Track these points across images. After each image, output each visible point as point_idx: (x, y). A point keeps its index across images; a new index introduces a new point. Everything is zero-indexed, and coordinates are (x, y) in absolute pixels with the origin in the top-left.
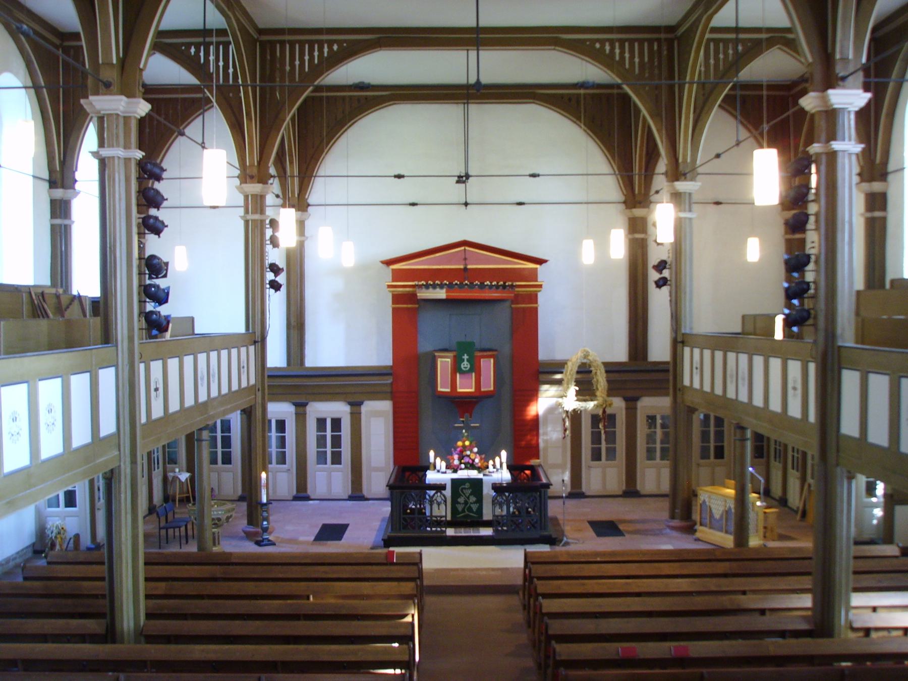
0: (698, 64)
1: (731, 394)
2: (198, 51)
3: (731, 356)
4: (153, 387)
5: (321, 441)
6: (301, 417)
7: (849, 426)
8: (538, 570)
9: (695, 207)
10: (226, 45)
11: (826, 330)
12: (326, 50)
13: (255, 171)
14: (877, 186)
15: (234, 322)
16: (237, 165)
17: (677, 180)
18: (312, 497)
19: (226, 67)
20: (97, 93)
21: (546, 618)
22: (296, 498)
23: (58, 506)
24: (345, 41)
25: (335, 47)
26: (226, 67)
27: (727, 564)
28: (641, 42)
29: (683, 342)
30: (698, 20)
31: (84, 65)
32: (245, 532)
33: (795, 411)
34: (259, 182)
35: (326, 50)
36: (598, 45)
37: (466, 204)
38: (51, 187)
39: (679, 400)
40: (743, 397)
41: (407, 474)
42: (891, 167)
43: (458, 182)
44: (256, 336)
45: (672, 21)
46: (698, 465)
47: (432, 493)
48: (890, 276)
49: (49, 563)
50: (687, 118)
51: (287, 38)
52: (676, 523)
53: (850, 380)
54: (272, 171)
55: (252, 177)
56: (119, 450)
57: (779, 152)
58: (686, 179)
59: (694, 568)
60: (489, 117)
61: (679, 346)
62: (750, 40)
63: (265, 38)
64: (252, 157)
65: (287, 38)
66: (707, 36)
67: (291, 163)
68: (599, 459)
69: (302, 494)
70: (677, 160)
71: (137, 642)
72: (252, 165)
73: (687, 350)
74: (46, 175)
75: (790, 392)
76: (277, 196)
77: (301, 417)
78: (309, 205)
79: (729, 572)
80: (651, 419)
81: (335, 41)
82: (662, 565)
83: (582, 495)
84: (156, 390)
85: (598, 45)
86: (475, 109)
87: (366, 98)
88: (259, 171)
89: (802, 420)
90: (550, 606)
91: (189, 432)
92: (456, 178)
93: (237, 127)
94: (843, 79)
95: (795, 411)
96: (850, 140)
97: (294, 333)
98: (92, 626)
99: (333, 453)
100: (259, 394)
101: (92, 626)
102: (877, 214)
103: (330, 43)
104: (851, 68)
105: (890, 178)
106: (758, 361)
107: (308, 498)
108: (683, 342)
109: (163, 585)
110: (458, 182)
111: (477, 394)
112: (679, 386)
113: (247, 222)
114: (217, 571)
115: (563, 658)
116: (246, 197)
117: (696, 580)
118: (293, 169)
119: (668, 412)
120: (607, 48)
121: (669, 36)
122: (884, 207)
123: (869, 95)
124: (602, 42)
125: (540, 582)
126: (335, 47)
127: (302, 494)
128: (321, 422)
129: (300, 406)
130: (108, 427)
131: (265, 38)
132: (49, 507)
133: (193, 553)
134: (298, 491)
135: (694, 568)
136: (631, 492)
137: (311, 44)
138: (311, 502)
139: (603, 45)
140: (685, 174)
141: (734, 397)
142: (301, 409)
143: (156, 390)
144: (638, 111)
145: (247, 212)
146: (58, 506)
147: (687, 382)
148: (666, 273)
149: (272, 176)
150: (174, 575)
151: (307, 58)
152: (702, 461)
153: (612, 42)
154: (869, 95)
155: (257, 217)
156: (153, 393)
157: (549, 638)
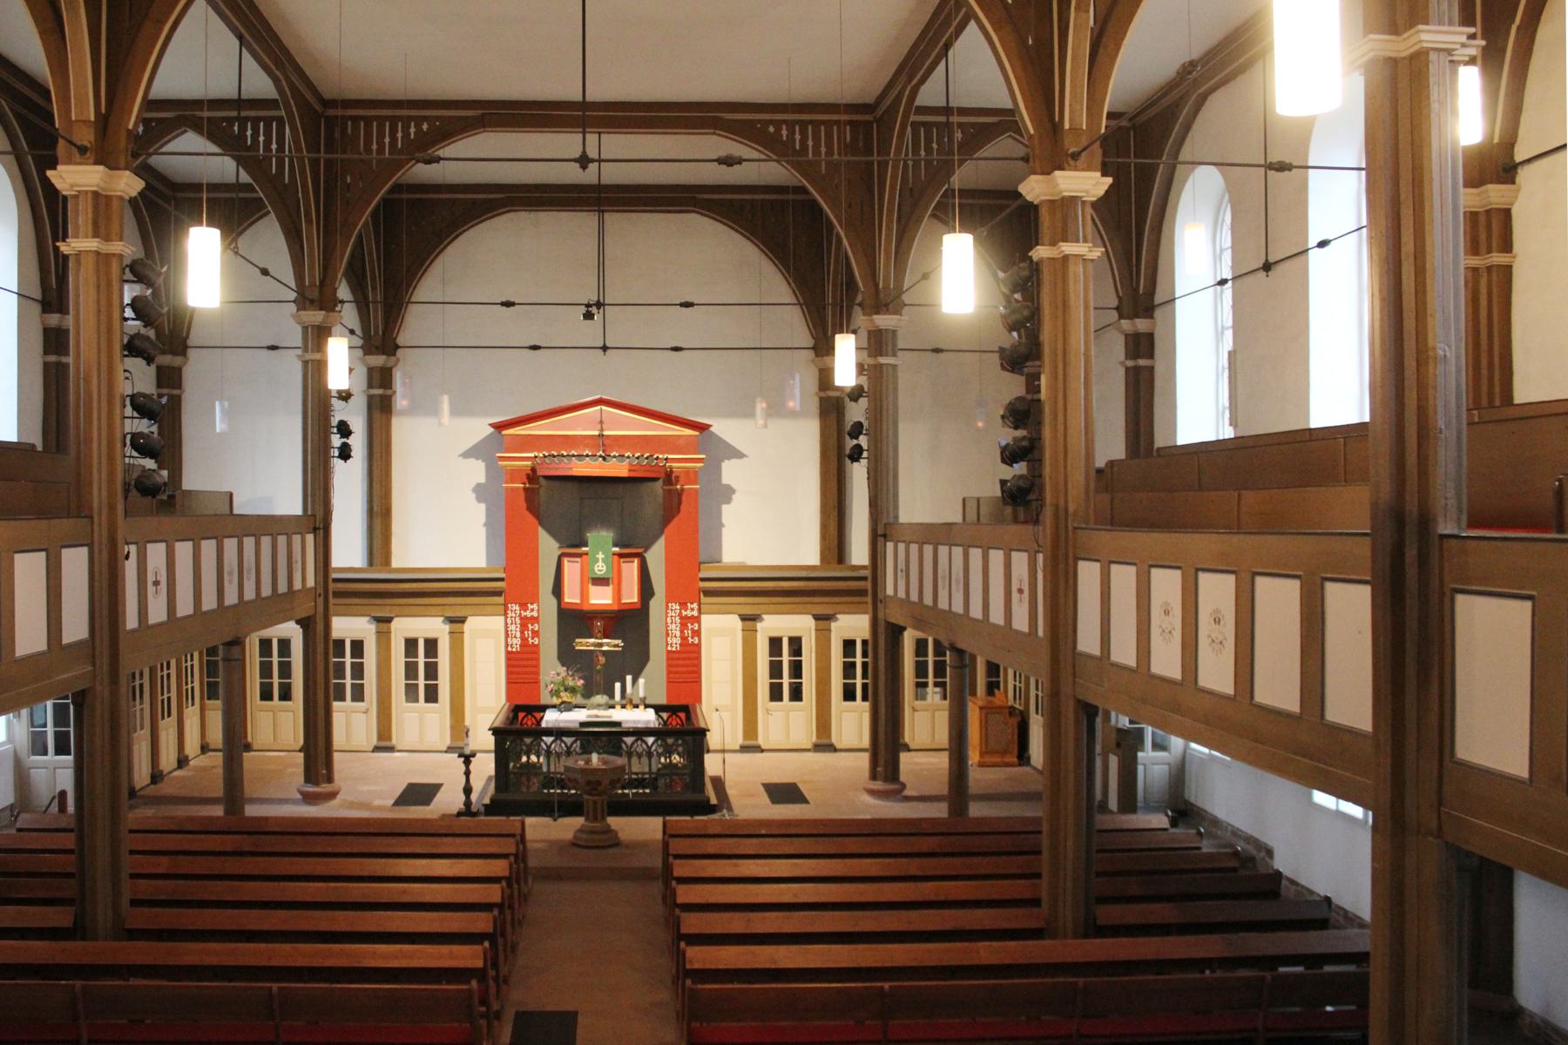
0: (902, 152)
1: (943, 604)
2: (243, 129)
3: (943, 550)
4: (150, 578)
5: (411, 670)
6: (384, 637)
7: (1088, 642)
8: (678, 846)
9: (900, 353)
10: (280, 121)
11: (1057, 507)
12: (412, 130)
13: (315, 294)
14: (1141, 325)
15: (289, 501)
16: (293, 285)
17: (877, 313)
18: (838, 746)
19: (281, 148)
20: (70, 162)
21: (677, 911)
22: (377, 749)
23: (45, 753)
24: (438, 118)
25: (425, 127)
26: (281, 148)
27: (936, 839)
28: (829, 124)
29: (884, 536)
30: (901, 93)
31: (53, 124)
32: (302, 793)
33: (1021, 623)
34: (96, 163)
35: (412, 130)
36: (771, 129)
37: (605, 348)
38: (44, 311)
39: (881, 615)
40: (958, 608)
41: (521, 715)
42: (1159, 298)
43: (588, 316)
44: (318, 520)
45: (870, 100)
46: (914, 710)
47: (549, 740)
48: (1159, 442)
49: (19, 830)
50: (889, 229)
51: (361, 112)
52: (879, 785)
53: (1088, 573)
54: (344, 292)
55: (312, 302)
56: (94, 665)
57: (975, 240)
58: (888, 312)
59: (891, 845)
60: (636, 233)
61: (881, 540)
62: (973, 125)
63: (331, 112)
64: (313, 274)
65: (361, 112)
66: (913, 118)
67: (374, 288)
68: (781, 699)
69: (384, 745)
70: (877, 285)
71: (116, 938)
72: (312, 284)
73: (890, 545)
74: (38, 294)
75: (1015, 596)
76: (352, 332)
77: (384, 637)
78: (398, 347)
79: (938, 850)
80: (849, 645)
81: (425, 118)
82: (846, 840)
83: (758, 749)
84: (156, 583)
85: (771, 129)
86: (614, 220)
87: (474, 202)
88: (321, 292)
89: (1030, 634)
90: (686, 894)
91: (210, 645)
92: (583, 309)
93: (293, 235)
94: (1075, 156)
95: (1021, 623)
96: (1085, 241)
97: (378, 522)
98: (59, 917)
99: (427, 686)
100: (321, 601)
101: (59, 917)
102: (1142, 362)
103: (419, 121)
104: (1084, 142)
105: (1158, 313)
106: (976, 554)
107: (391, 749)
108: (884, 536)
109: (164, 860)
110: (588, 316)
111: (616, 608)
112: (880, 596)
113: (305, 363)
114: (246, 843)
115: (696, 966)
116: (305, 329)
117: (887, 860)
118: (376, 295)
119: (867, 635)
120: (784, 132)
121: (867, 117)
122: (1150, 354)
123: (1109, 180)
124: (778, 124)
125: (678, 861)
126: (425, 127)
127: (384, 745)
128: (411, 644)
129: (823, 619)
130: (75, 627)
131: (331, 112)
132: (34, 754)
133: (218, 818)
134: (380, 738)
135: (891, 845)
136: (824, 746)
137: (394, 121)
138: (397, 754)
139: (778, 130)
140: (886, 305)
141: (946, 607)
142: (384, 626)
143: (156, 583)
144: (831, 227)
145: (305, 349)
146: (45, 753)
147: (890, 591)
148: (863, 441)
149: (342, 302)
150: (187, 847)
151: (387, 140)
152: (918, 703)
153: (791, 125)
154: (1109, 180)
155: (379, 392)
156: (151, 589)
157: (682, 937)
